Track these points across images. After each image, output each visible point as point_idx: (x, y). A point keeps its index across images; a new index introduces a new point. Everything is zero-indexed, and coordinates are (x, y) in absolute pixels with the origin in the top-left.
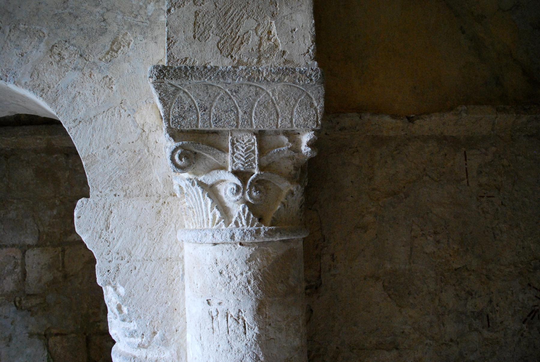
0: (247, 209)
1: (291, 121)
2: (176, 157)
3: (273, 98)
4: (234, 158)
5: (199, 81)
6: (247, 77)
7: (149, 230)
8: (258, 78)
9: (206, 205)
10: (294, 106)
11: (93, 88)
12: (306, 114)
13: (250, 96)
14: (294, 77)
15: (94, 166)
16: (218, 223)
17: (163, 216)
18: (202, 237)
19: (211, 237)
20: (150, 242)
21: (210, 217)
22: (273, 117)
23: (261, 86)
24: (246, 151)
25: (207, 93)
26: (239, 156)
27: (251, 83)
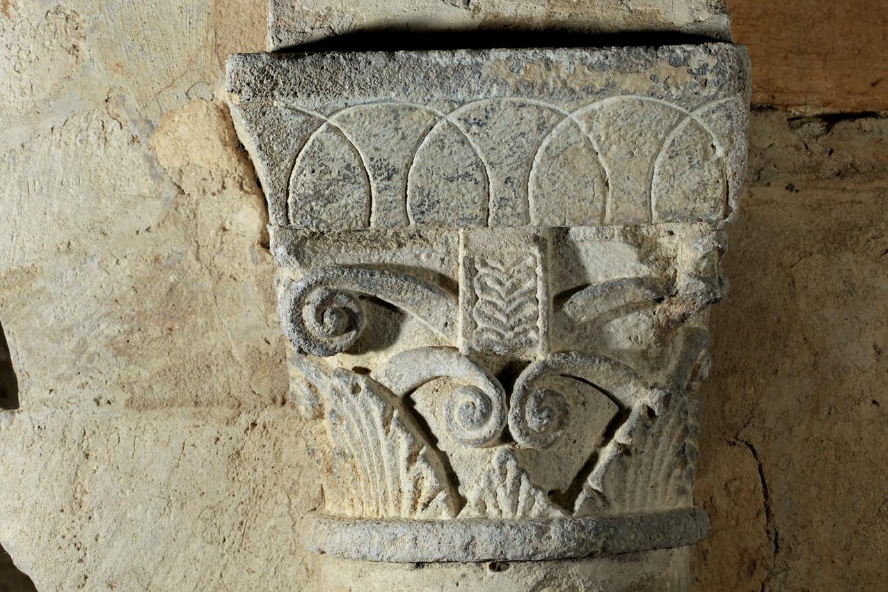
0: (511, 465)
1: (647, 204)
2: (308, 313)
3: (591, 137)
4: (475, 315)
5: (373, 98)
6: (511, 81)
7: (209, 514)
8: (545, 84)
9: (393, 450)
10: (655, 157)
11: (14, 50)
12: (691, 180)
13: (523, 134)
14: (653, 78)
15: (27, 309)
16: (426, 506)
17: (250, 469)
18: (382, 544)
19: (408, 545)
20: (211, 549)
21: (407, 486)
22: (590, 191)
23: (553, 106)
24: (509, 292)
25: (396, 129)
26: (488, 310)
27: (524, 99)
